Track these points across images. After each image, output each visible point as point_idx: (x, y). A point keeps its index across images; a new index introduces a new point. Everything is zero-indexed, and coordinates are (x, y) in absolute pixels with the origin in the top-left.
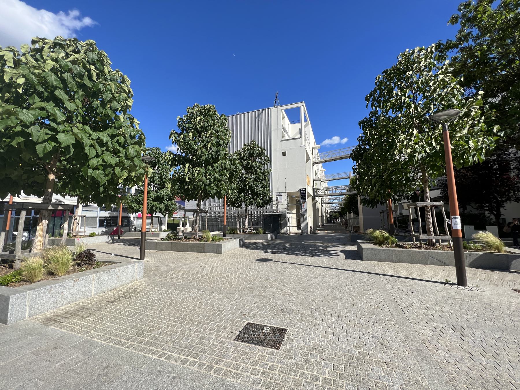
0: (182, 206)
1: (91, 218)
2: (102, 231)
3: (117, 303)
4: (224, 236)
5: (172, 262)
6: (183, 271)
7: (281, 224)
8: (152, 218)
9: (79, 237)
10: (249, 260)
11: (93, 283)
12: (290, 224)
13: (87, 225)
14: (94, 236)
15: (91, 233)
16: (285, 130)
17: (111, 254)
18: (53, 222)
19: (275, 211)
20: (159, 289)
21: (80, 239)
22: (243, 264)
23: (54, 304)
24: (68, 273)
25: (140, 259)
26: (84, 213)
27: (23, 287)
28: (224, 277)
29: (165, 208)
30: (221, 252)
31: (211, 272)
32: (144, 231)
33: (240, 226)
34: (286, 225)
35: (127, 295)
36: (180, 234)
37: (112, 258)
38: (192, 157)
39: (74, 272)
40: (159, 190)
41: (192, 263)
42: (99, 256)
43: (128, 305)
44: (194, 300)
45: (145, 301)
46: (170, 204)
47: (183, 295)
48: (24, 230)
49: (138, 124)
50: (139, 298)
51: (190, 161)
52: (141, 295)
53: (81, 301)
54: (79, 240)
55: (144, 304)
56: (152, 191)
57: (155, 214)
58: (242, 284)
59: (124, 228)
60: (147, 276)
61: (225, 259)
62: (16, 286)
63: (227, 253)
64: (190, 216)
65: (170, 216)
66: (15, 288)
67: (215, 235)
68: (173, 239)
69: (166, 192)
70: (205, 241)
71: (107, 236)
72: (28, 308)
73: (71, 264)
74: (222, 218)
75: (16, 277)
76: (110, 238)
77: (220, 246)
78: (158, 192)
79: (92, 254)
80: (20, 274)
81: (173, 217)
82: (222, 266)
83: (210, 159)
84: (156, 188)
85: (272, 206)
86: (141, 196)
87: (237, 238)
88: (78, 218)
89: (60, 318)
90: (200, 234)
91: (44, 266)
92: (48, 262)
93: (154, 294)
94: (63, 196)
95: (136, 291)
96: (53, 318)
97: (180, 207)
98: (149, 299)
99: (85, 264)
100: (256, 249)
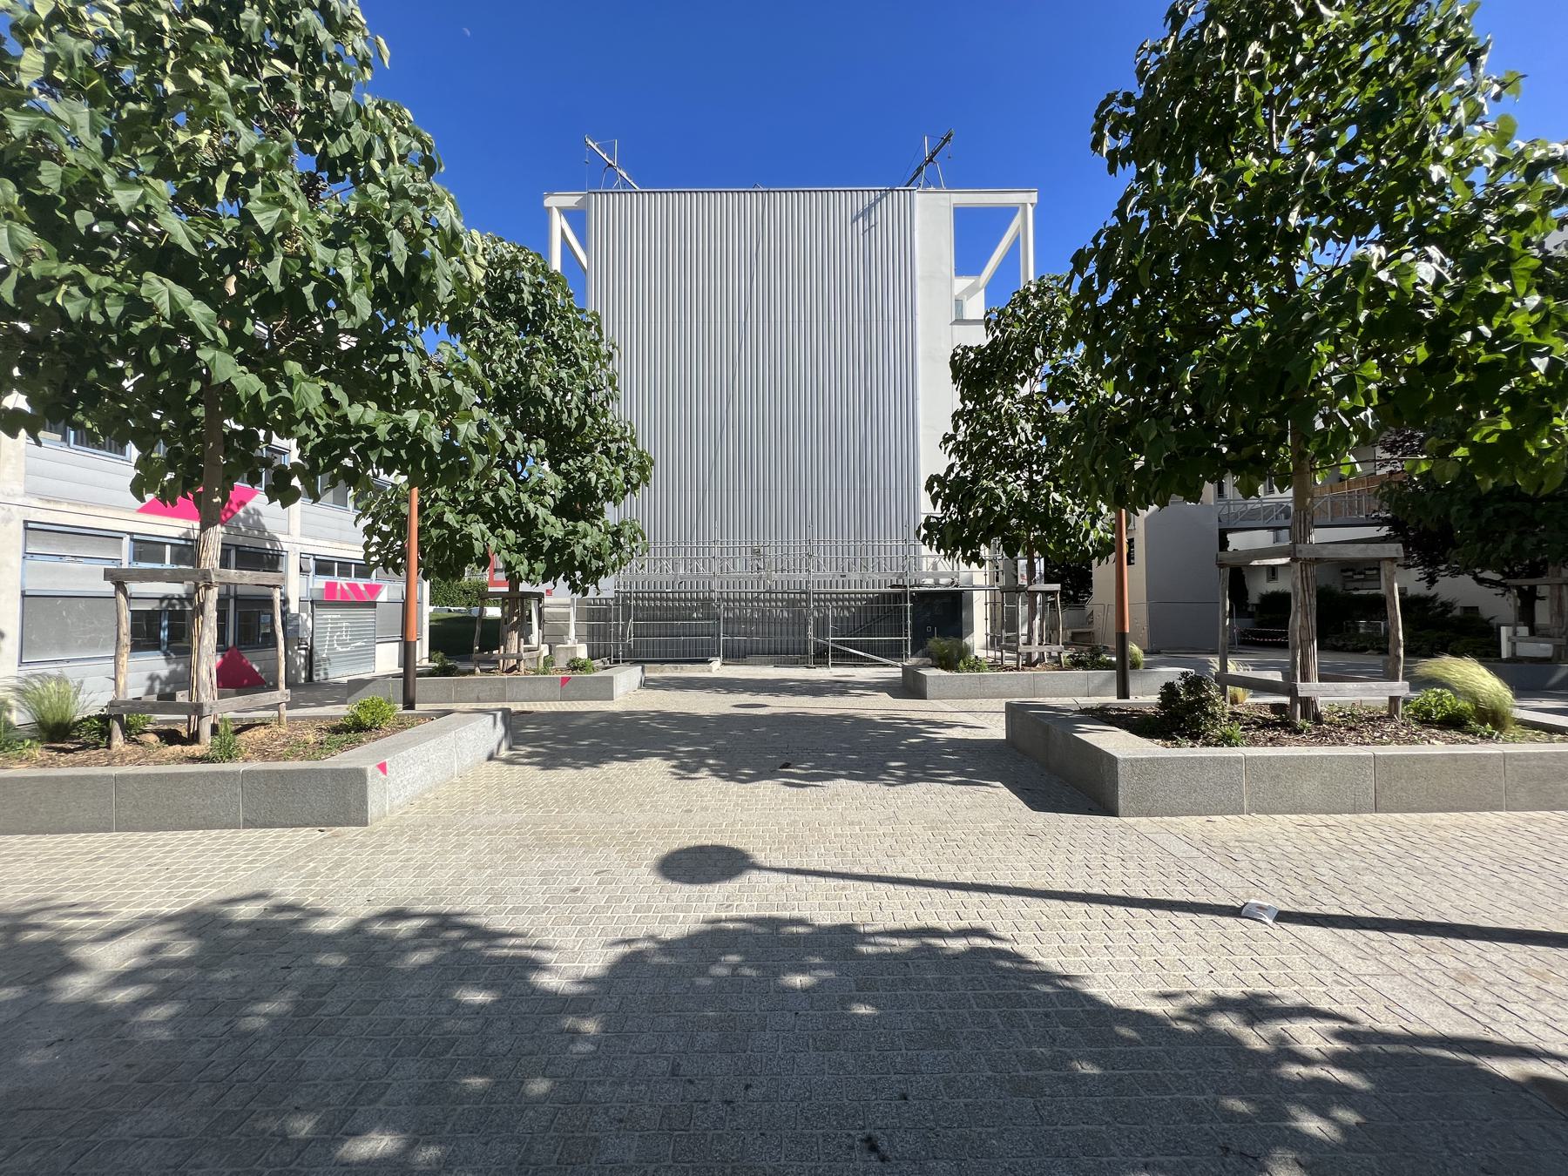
1: (82, 604)
2: (152, 678)
19: (930, 581)
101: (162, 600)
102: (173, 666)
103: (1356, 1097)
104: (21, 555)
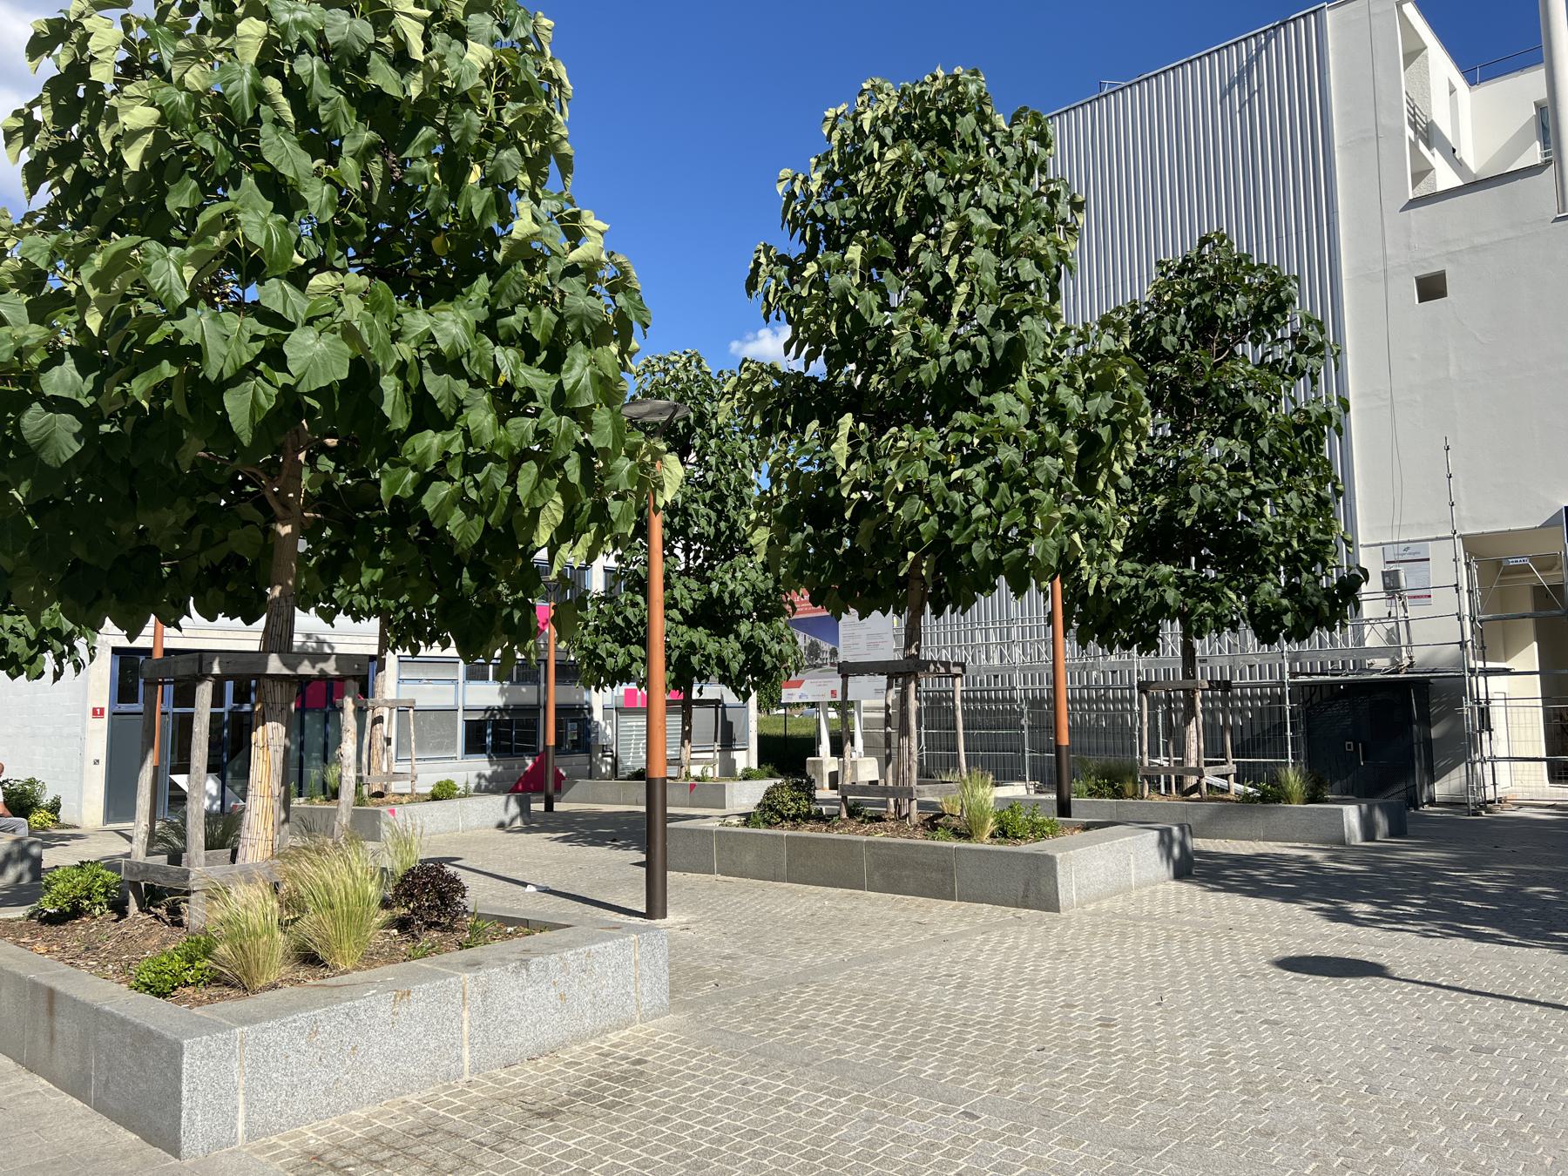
0: (826, 646)
1: (432, 715)
2: (480, 776)
3: (567, 1124)
4: (1064, 809)
5: (799, 942)
6: (853, 990)
7: (1428, 742)
8: (686, 707)
9: (396, 803)
10: (1227, 959)
11: (466, 1014)
12: (1498, 742)
13: (420, 747)
14: (450, 796)
15: (439, 785)
16: (1428, 134)
17: (525, 884)
18: (297, 732)
19: (1382, 663)
20: (745, 1075)
21: (397, 809)
22: (1193, 983)
23: (327, 1092)
24: (369, 959)
25: (649, 915)
26: (409, 692)
27: (221, 1006)
28: (1084, 1046)
29: (742, 657)
30: (1049, 903)
31: (1008, 1012)
32: (658, 772)
33: (1154, 753)
34: (1463, 747)
35: (605, 1089)
36: (824, 792)
37: (527, 903)
38: (866, 380)
39: (391, 960)
40: (712, 567)
41: (897, 952)
42: (479, 894)
43: (612, 1138)
44: (927, 1159)
45: (688, 1127)
46: (766, 638)
47: (870, 1120)
48: (211, 769)
49: (602, 233)
50: (658, 1112)
51: (857, 401)
52: (664, 1095)
53: (424, 1094)
54: (393, 812)
55: (685, 1146)
56: (681, 574)
57: (700, 691)
58: (1201, 1099)
59: (567, 760)
60: (687, 1005)
61: (1081, 943)
62: (200, 1003)
63: (1091, 907)
64: (871, 695)
65: (770, 701)
66: (197, 1011)
67: (1012, 805)
68: (794, 818)
69: (744, 578)
70: (958, 834)
71: (502, 799)
72: (241, 1098)
73: (377, 920)
74: (1045, 709)
75: (197, 964)
76: (514, 809)
77: (1045, 866)
78: (709, 581)
79: (454, 880)
80: (207, 952)
81: (781, 706)
82: (1069, 979)
83: (967, 376)
84: (696, 557)
85: (1358, 630)
86: (635, 604)
87: (1145, 824)
88: (385, 712)
89: (351, 1160)
90: (929, 794)
91: (283, 925)
92: (293, 905)
93: (725, 1101)
94: (328, 617)
95: (642, 1073)
96: (329, 1157)
97: (814, 650)
98: (704, 1122)
99: (430, 925)
100: (1258, 890)
101: (486, 711)
102: (495, 767)
103: (312, 270)
104: (396, 681)
